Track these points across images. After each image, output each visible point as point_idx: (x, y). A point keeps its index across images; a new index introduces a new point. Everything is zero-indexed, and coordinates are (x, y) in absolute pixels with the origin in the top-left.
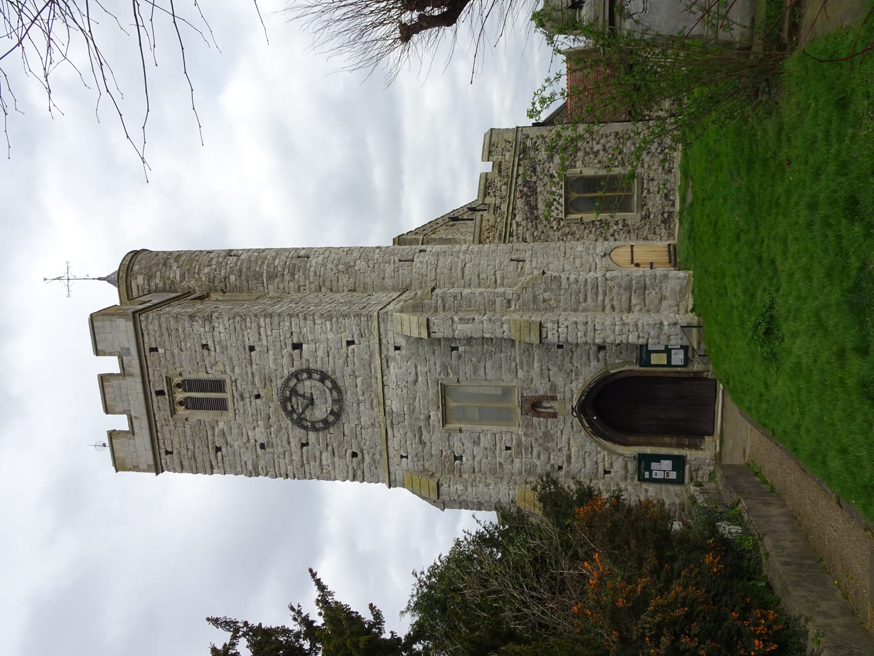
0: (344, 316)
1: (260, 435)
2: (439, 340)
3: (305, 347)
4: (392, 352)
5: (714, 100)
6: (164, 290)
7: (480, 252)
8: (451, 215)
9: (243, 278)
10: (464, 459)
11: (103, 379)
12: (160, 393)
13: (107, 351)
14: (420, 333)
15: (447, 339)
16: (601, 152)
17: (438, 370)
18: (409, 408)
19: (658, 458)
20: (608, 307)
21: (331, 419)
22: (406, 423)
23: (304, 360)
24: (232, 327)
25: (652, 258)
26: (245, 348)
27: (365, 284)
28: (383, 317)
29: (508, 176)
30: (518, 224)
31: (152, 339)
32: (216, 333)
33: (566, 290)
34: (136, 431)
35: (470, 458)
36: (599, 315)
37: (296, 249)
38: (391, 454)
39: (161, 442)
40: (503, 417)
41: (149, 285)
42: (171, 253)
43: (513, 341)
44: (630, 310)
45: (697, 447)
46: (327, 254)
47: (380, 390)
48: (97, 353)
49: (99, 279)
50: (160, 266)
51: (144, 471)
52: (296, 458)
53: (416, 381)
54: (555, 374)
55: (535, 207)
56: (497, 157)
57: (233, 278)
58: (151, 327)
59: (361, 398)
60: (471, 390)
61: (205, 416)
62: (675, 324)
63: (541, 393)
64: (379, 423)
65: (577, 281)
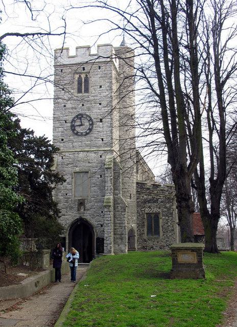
30: (143, 197)
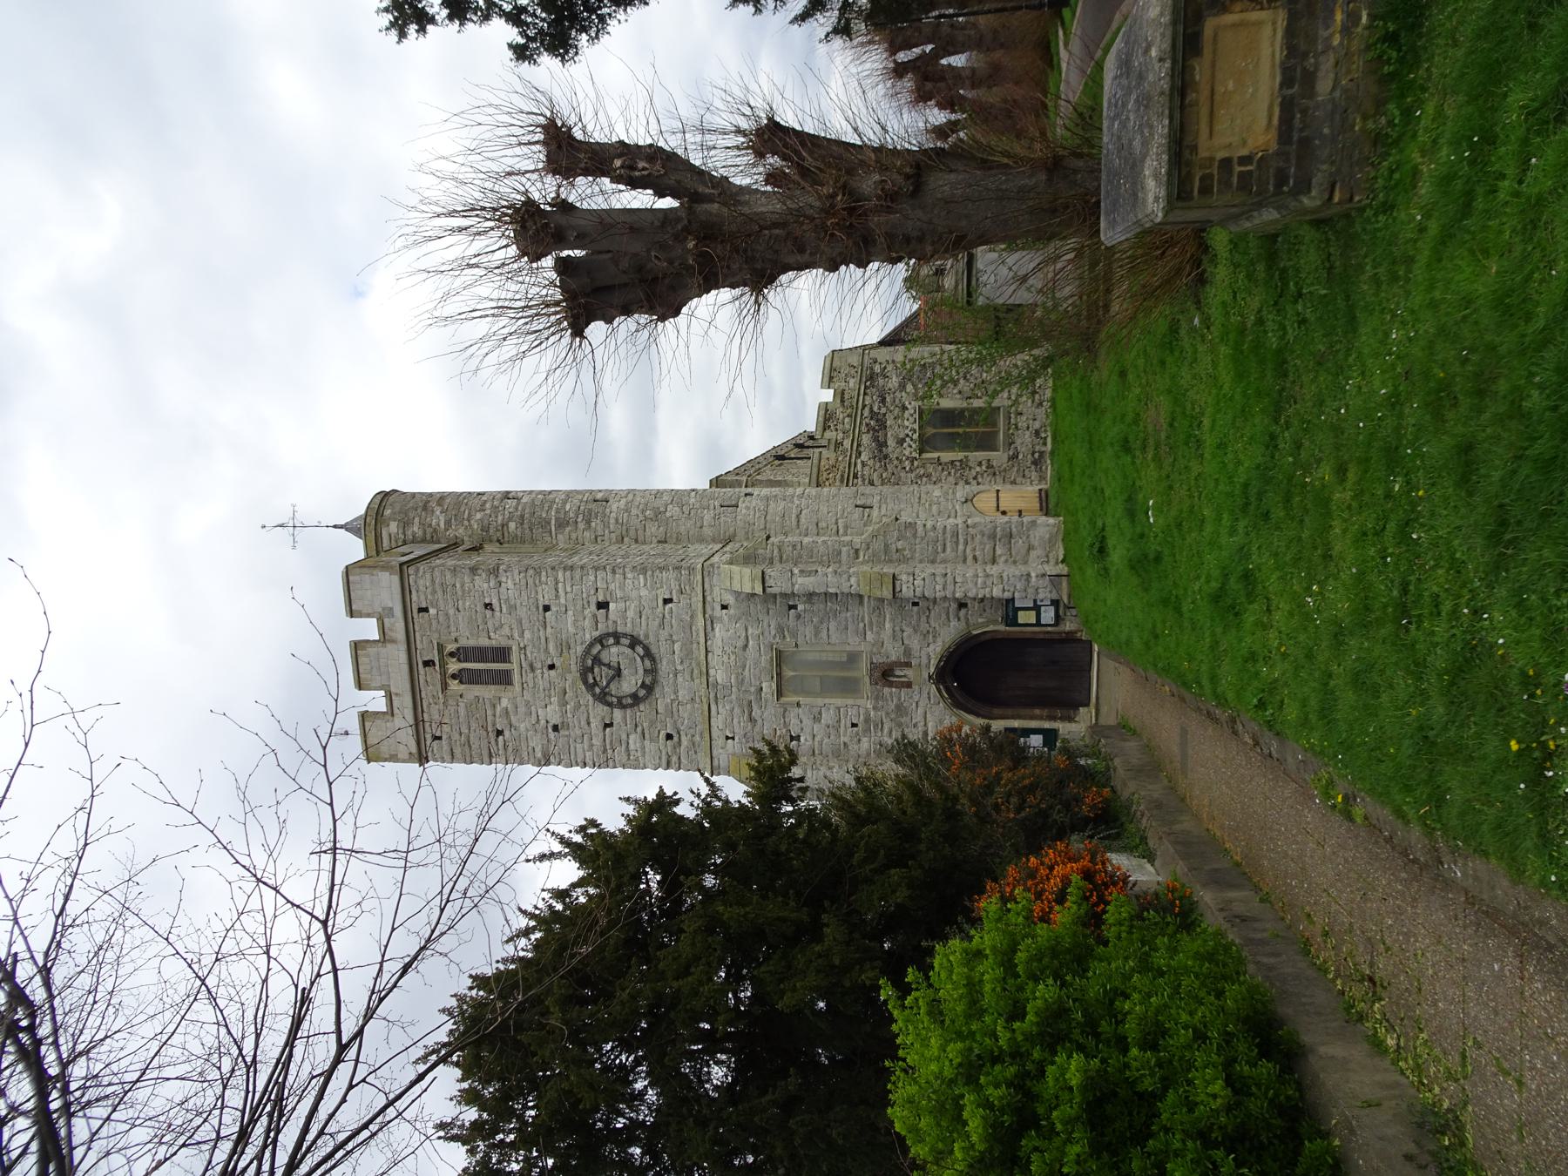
0: (662, 569)
1: (552, 714)
2: (775, 596)
3: (612, 606)
4: (718, 612)
5: (1048, 361)
6: (424, 541)
7: (818, 496)
8: (774, 453)
9: (526, 526)
10: (802, 739)
11: (357, 647)
12: (428, 663)
13: (364, 611)
14: (753, 588)
15: (784, 595)
16: (962, 381)
17: (773, 633)
18: (737, 678)
19: (1027, 732)
20: (970, 558)
21: (642, 693)
22: (733, 697)
23: (610, 622)
24: (523, 582)
25: (1020, 505)
26: (538, 608)
27: (679, 533)
28: (707, 570)
29: (852, 407)
30: (864, 464)
31: (422, 597)
32: (503, 590)
33: (923, 539)
34: (396, 711)
35: (810, 738)
36: (960, 567)
37: (591, 492)
38: (714, 735)
39: (427, 725)
40: (848, 687)
41: (404, 533)
42: (431, 495)
43: (861, 597)
44: (994, 561)
45: (1070, 719)
46: (630, 497)
47: (703, 657)
48: (352, 613)
49: (335, 527)
50: (419, 510)
51: (404, 761)
52: (597, 742)
53: (746, 646)
54: (910, 636)
55: (885, 444)
56: (841, 385)
57: (512, 525)
58: (421, 582)
59: (679, 667)
60: (810, 657)
61: (486, 692)
62: (1044, 575)
63: (893, 658)
64: (700, 697)
65: (934, 528)
